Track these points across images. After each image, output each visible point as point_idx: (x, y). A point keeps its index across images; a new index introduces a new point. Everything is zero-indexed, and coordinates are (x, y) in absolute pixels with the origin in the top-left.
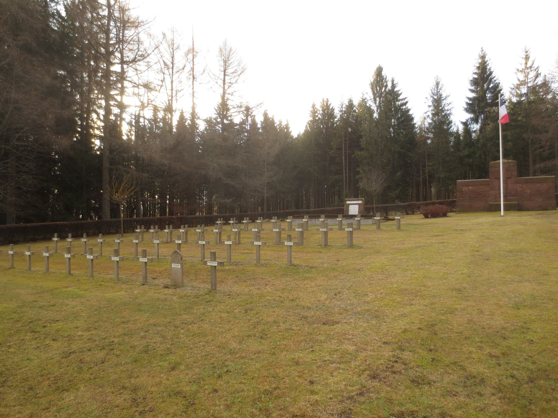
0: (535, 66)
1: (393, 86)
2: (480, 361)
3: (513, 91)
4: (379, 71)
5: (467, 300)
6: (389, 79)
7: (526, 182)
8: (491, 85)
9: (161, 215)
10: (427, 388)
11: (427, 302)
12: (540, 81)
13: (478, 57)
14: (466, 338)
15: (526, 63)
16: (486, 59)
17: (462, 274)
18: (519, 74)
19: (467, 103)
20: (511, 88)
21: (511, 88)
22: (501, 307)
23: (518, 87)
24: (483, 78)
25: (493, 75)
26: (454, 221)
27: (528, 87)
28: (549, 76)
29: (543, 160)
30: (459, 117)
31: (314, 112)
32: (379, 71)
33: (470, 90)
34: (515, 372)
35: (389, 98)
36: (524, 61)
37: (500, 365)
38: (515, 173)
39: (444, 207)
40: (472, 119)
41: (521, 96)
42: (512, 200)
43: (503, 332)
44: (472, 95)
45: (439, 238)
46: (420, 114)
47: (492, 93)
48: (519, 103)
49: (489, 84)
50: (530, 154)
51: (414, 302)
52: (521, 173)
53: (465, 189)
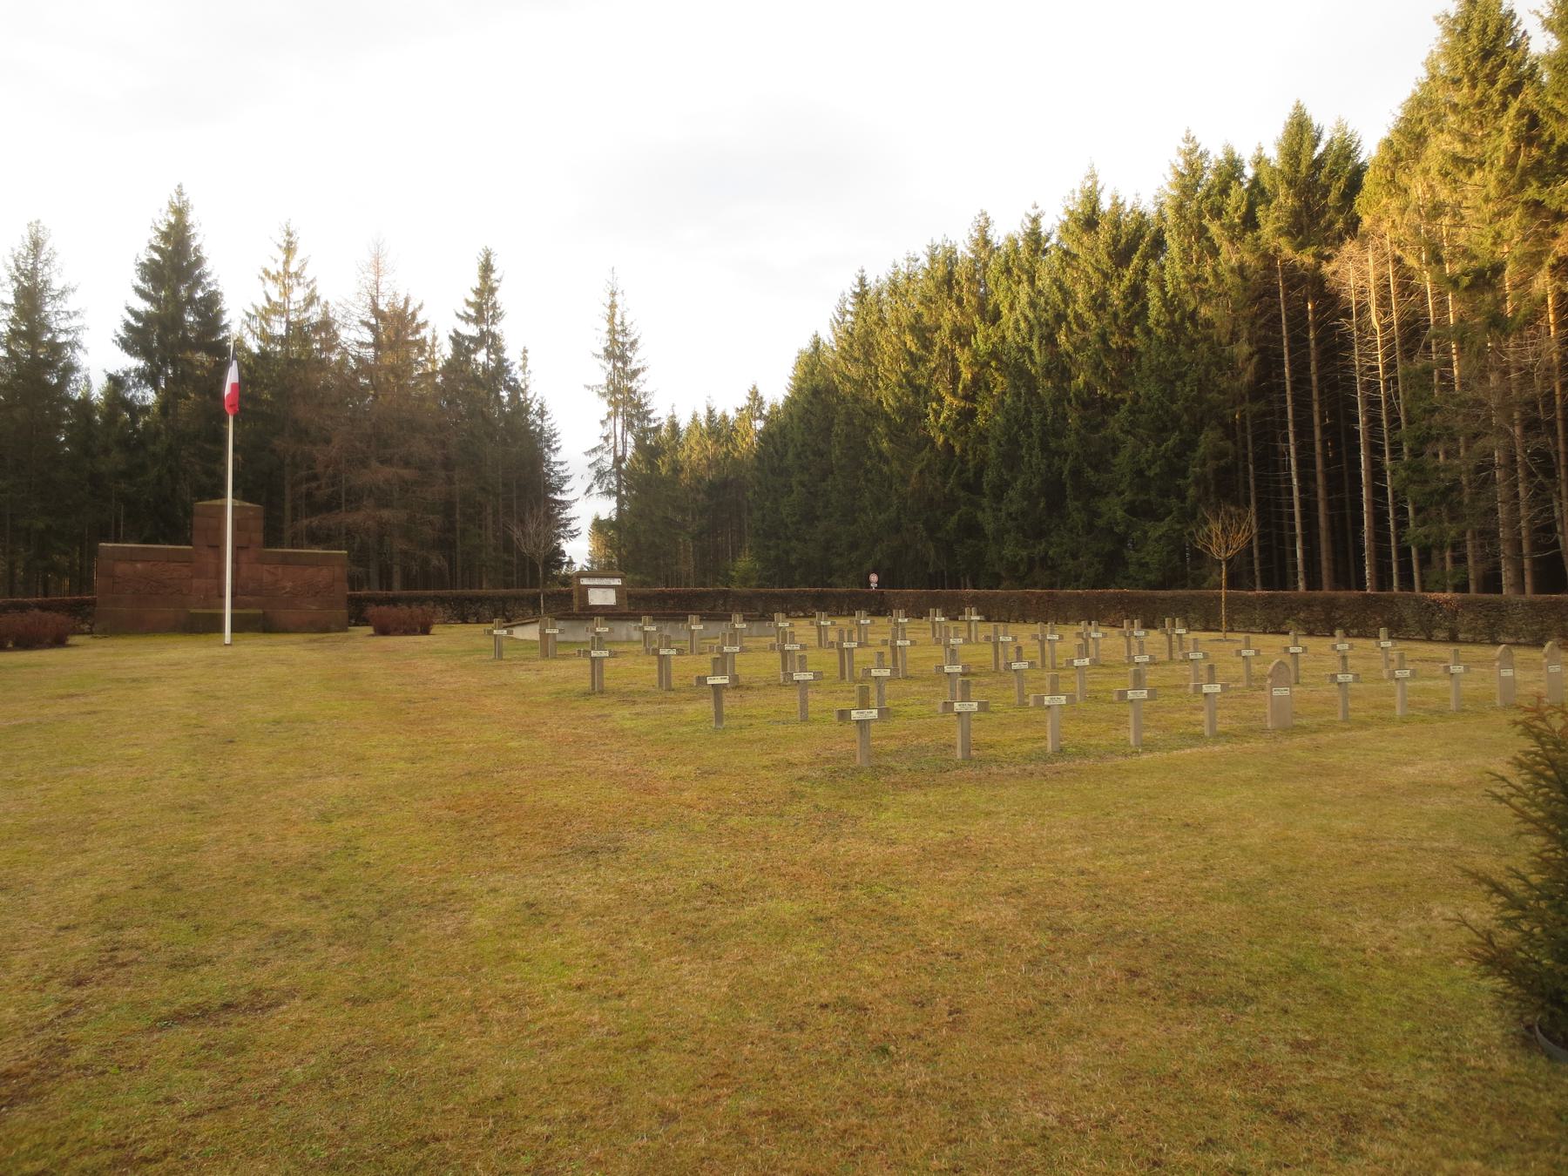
2: (289, 910)
3: (254, 324)
5: (217, 824)
7: (285, 560)
8: (199, 294)
9: (1308, 589)
10: (207, 968)
11: (121, 840)
12: (315, 315)
13: (166, 207)
14: (247, 884)
15: (287, 262)
17: (183, 776)
18: (270, 283)
19: (128, 326)
20: (248, 315)
21: (248, 315)
22: (295, 824)
23: (265, 316)
24: (173, 266)
26: (89, 657)
27: (289, 323)
28: (339, 309)
29: (315, 508)
30: (100, 359)
33: (137, 289)
34: (355, 910)
36: (282, 257)
37: (326, 907)
38: (259, 537)
39: (60, 618)
40: (141, 374)
41: (267, 338)
42: (248, 605)
43: (314, 861)
44: (143, 306)
45: (75, 701)
47: (197, 313)
48: (264, 355)
49: (192, 289)
50: (287, 491)
51: (87, 845)
52: (273, 535)
53: (122, 568)
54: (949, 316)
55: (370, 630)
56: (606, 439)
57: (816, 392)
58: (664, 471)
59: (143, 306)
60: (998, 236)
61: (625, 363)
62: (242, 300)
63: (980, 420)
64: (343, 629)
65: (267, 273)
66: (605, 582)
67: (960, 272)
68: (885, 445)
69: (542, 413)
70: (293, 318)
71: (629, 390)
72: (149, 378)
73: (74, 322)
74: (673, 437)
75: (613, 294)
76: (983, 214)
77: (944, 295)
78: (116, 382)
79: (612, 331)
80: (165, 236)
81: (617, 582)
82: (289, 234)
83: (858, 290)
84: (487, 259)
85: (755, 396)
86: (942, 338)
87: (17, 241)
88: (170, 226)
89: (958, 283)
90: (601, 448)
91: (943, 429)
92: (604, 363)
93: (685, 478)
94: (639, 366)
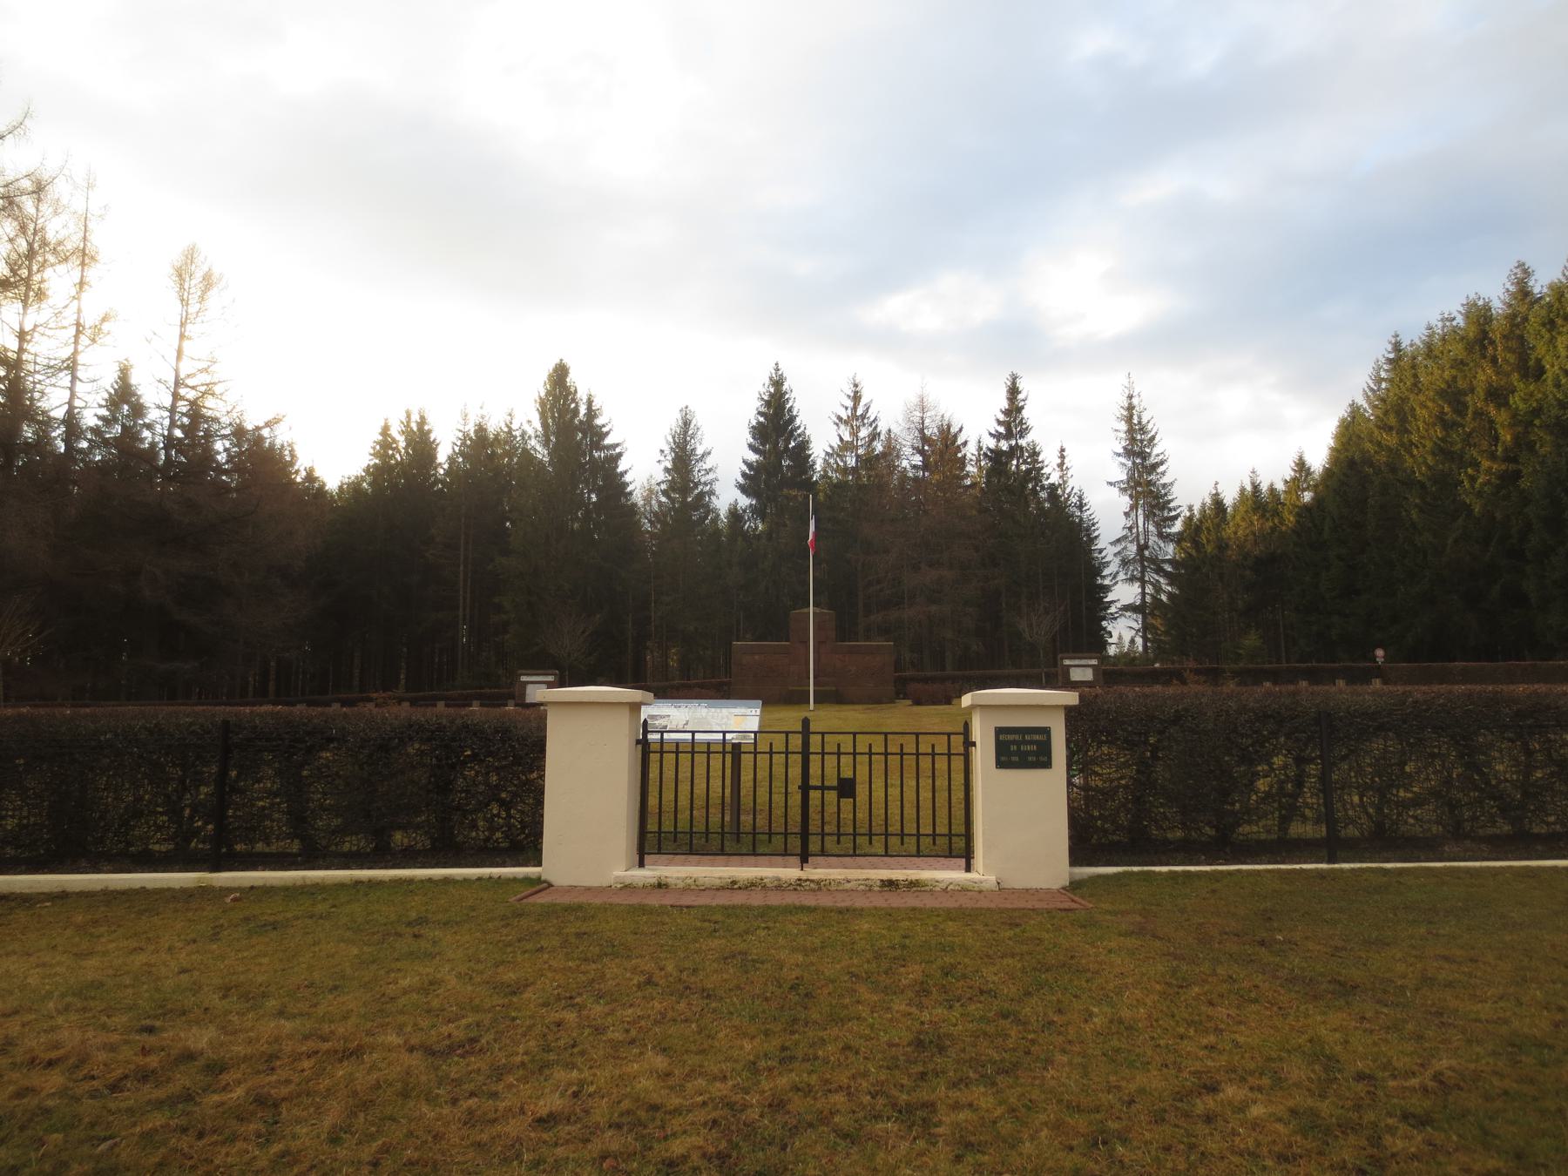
0: (872, 415)
1: (592, 414)
4: (560, 374)
6: (582, 395)
13: (767, 382)
15: (855, 408)
16: (785, 387)
18: (842, 427)
19: (744, 475)
24: (776, 424)
25: (798, 422)
27: (858, 456)
30: (727, 495)
31: (386, 443)
32: (560, 374)
35: (572, 426)
36: (850, 404)
41: (845, 470)
44: (753, 457)
46: (643, 469)
54: (1484, 376)
55: (909, 702)
56: (1130, 529)
57: (1352, 463)
58: (1209, 549)
59: (753, 457)
60: (1540, 285)
61: (1144, 459)
62: (822, 437)
63: (1524, 483)
64: (892, 701)
65: (840, 418)
66: (1083, 662)
67: (1497, 330)
68: (1414, 514)
69: (1081, 506)
70: (861, 451)
71: (1150, 483)
72: (758, 511)
73: (711, 476)
74: (1217, 515)
75: (1130, 397)
76: (1521, 265)
77: (1477, 356)
78: (734, 514)
79: (1131, 431)
80: (768, 404)
81: (1094, 662)
82: (856, 386)
83: (1392, 356)
84: (1014, 383)
85: (1301, 465)
86: (1475, 401)
87: (672, 422)
88: (771, 395)
89: (1492, 342)
90: (1125, 537)
91: (1479, 494)
92: (1123, 460)
93: (1232, 554)
94: (1158, 460)
